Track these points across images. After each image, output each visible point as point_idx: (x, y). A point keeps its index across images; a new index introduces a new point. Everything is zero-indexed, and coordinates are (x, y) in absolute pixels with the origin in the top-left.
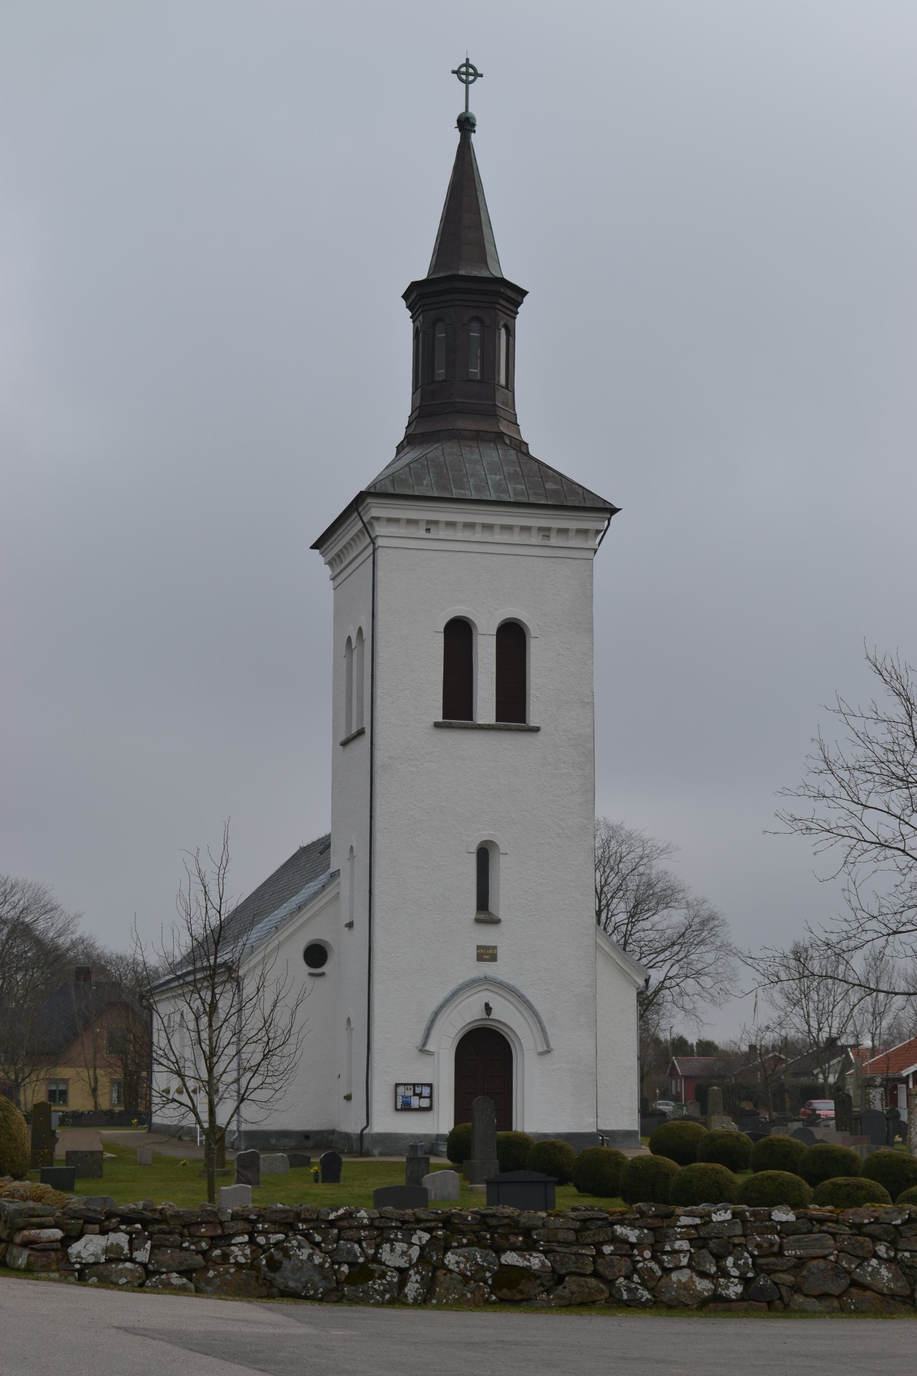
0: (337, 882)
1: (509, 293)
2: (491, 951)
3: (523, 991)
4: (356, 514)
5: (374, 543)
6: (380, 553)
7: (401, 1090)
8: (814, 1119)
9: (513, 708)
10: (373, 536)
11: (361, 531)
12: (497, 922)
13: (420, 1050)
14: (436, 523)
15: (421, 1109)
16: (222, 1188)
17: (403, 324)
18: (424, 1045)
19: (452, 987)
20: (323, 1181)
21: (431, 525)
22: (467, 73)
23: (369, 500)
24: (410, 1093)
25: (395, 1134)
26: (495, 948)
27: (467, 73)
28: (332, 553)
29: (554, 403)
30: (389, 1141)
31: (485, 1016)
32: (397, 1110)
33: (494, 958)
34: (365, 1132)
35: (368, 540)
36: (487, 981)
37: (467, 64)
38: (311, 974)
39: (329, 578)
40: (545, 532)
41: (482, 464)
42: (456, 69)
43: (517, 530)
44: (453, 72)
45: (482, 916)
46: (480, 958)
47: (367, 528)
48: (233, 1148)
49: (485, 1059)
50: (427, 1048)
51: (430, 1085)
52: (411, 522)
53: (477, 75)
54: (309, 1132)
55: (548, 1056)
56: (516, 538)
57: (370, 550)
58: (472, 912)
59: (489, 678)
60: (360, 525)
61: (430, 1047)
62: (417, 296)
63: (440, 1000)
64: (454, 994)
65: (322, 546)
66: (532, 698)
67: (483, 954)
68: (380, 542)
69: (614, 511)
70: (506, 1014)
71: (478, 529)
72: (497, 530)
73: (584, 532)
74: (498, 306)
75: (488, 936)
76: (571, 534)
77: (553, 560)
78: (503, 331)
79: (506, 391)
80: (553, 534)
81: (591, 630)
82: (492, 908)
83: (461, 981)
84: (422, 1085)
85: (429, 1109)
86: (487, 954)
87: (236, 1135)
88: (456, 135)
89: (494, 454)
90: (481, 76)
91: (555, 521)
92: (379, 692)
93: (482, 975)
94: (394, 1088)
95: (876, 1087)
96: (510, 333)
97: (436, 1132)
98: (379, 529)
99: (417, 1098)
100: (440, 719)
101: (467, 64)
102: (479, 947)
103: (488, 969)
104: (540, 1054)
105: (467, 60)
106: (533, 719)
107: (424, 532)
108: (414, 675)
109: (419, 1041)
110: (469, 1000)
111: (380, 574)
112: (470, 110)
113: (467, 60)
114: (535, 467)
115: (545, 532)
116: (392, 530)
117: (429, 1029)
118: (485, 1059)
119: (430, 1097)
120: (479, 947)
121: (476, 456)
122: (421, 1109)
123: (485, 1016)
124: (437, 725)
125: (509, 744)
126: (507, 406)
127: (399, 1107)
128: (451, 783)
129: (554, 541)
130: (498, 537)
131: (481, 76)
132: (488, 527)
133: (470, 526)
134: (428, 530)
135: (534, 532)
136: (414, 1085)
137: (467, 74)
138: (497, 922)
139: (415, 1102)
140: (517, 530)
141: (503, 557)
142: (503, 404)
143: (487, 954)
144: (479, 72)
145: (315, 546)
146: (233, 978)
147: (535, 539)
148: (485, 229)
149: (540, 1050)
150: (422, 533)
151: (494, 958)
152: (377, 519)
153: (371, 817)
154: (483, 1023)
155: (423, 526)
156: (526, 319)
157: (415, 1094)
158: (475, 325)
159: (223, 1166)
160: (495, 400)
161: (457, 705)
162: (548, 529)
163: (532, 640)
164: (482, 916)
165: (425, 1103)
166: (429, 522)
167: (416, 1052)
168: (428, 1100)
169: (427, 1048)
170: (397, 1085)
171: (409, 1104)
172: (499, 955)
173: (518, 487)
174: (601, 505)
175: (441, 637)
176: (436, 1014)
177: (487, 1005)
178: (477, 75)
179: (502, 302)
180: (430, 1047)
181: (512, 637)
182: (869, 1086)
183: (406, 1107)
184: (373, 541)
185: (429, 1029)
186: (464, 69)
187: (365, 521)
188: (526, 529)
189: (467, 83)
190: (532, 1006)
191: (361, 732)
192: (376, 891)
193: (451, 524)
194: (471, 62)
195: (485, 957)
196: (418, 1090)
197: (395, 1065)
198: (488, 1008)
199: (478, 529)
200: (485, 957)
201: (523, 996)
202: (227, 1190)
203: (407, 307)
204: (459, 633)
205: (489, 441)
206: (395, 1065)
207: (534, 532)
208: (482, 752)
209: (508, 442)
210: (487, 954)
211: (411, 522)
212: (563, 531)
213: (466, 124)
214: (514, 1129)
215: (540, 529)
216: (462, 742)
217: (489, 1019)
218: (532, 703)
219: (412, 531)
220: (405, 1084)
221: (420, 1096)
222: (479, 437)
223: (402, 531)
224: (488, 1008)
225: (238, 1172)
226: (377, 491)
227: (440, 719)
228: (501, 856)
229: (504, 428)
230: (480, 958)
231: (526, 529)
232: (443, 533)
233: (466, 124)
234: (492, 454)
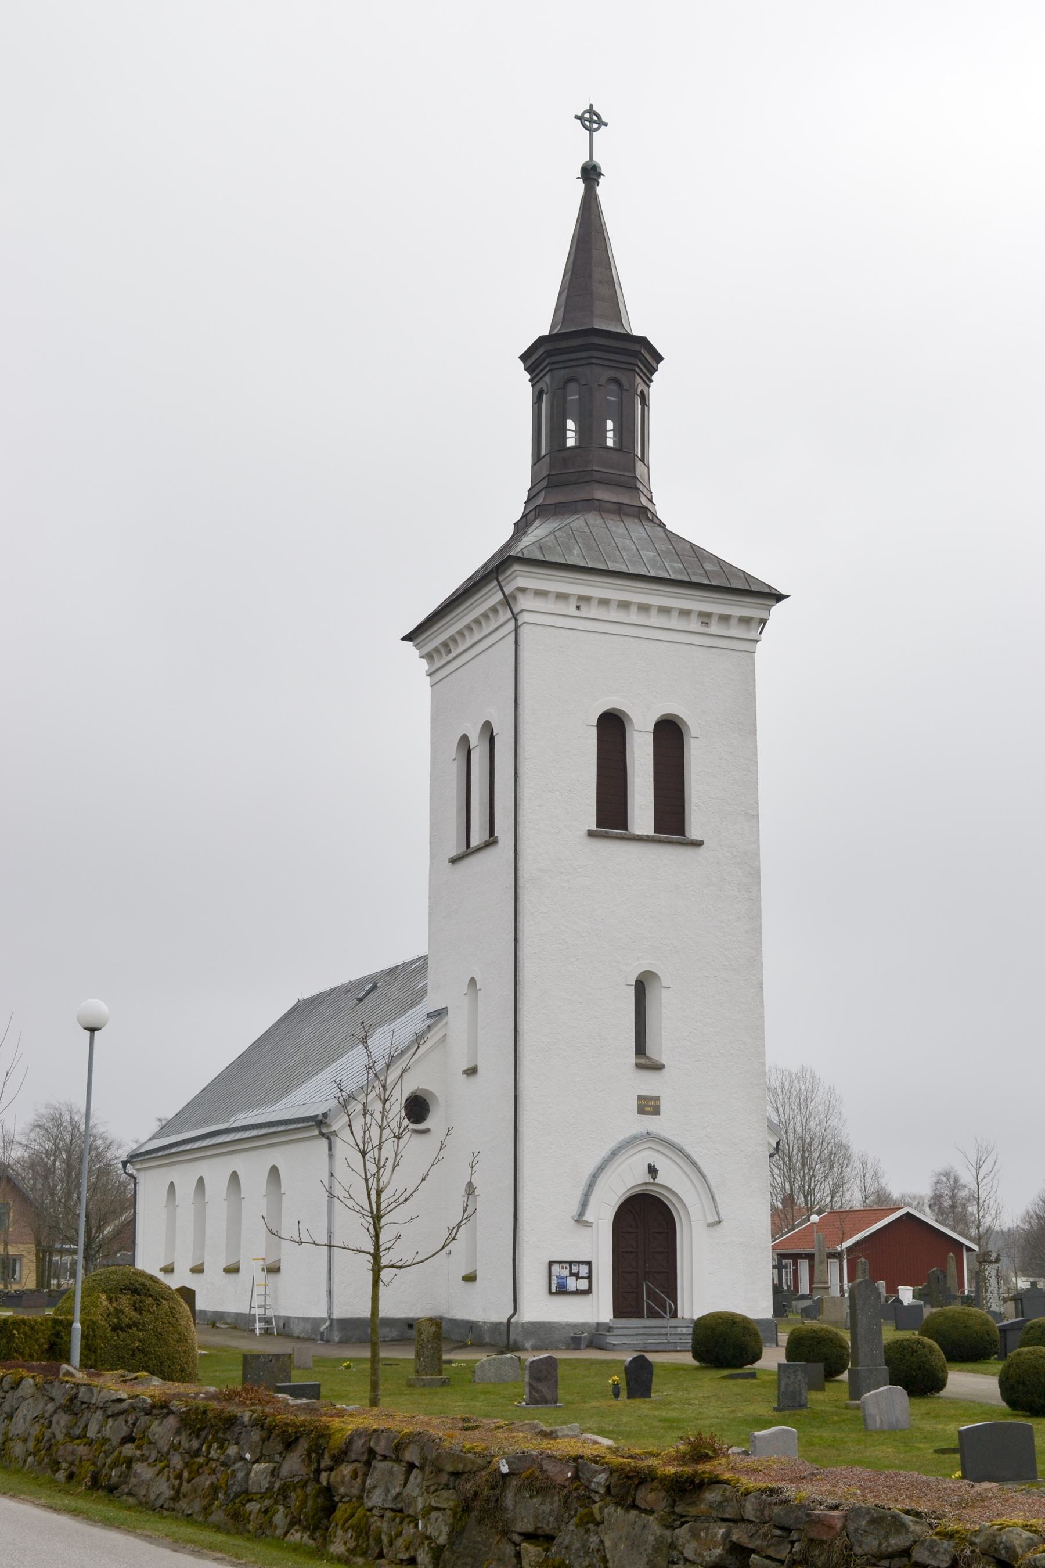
0: (444, 1022)
2: (653, 1103)
3: (688, 1149)
4: (495, 583)
5: (516, 620)
6: (524, 631)
9: (671, 819)
10: (516, 610)
11: (500, 603)
13: (577, 1221)
14: (587, 599)
16: (757, 1433)
17: (520, 387)
18: (582, 1213)
19: (612, 1145)
20: (630, 1396)
22: (591, 120)
23: (516, 567)
24: (566, 1273)
25: (549, 1323)
26: (657, 1098)
27: (591, 120)
28: (429, 648)
30: (543, 1333)
32: (551, 1293)
33: (656, 1111)
34: (512, 1320)
35: (509, 615)
36: (650, 1137)
37: (591, 111)
39: (424, 673)
40: (705, 617)
41: (624, 541)
44: (577, 117)
45: (643, 1061)
46: (641, 1111)
47: (508, 601)
48: (322, 1340)
49: (646, 1231)
50: (585, 1218)
51: (589, 1263)
52: (562, 597)
53: (601, 123)
54: (413, 1319)
55: (718, 1228)
57: (511, 625)
58: (630, 1056)
59: (647, 782)
60: (499, 596)
61: (588, 1217)
62: (540, 358)
63: (597, 1161)
64: (614, 1154)
65: (417, 637)
66: (693, 807)
67: (645, 1106)
68: (524, 617)
69: (779, 597)
70: (673, 1179)
72: (654, 612)
73: (746, 621)
75: (649, 1084)
77: (712, 650)
78: (638, 400)
80: (714, 621)
81: (754, 732)
82: (648, 1053)
84: (579, 1262)
85: (588, 1292)
86: (649, 1106)
87: (327, 1324)
88: (579, 188)
89: (641, 530)
90: (606, 124)
91: (717, 606)
92: (525, 793)
95: (991, 1262)
96: (644, 402)
97: (595, 1320)
98: (524, 602)
99: (574, 1278)
100: (594, 827)
101: (591, 111)
102: (640, 1098)
104: (710, 1225)
105: (591, 106)
106: (694, 829)
107: (575, 608)
108: (560, 778)
109: (575, 1209)
110: (627, 1163)
111: (525, 654)
112: (595, 159)
113: (591, 106)
114: (688, 547)
115: (705, 617)
116: (538, 604)
118: (646, 1231)
119: (589, 1278)
120: (640, 1098)
121: (622, 530)
124: (591, 834)
127: (554, 1290)
128: (606, 902)
129: (715, 628)
130: (655, 620)
131: (606, 124)
132: (644, 608)
133: (624, 605)
134: (578, 608)
136: (570, 1263)
137: (591, 121)
138: (658, 1067)
139: (572, 1284)
140: (675, 614)
143: (649, 1106)
145: (408, 638)
146: (323, 1135)
147: (694, 625)
149: (710, 1221)
150: (572, 610)
151: (656, 1111)
152: (523, 590)
153: (516, 940)
154: (644, 1188)
155: (573, 602)
156: (661, 387)
157: (571, 1274)
158: (613, 387)
159: (440, 1372)
161: (612, 814)
162: (709, 615)
163: (692, 741)
164: (643, 1061)
165: (583, 1285)
167: (573, 1222)
168: (586, 1281)
169: (585, 1218)
170: (589, 1263)
171: (564, 1286)
173: (675, 565)
174: (767, 590)
175: (594, 732)
176: (594, 1177)
178: (601, 123)
181: (670, 734)
182: (985, 1261)
183: (562, 1291)
184: (515, 617)
186: (587, 115)
187: (507, 593)
188: (685, 613)
189: (591, 131)
191: (492, 841)
192: (523, 1028)
193: (604, 602)
194: (595, 109)
195: (647, 1109)
196: (575, 1269)
198: (652, 1170)
199: (634, 609)
200: (647, 1109)
202: (762, 1437)
203: (526, 369)
204: (612, 727)
207: (694, 617)
208: (639, 865)
210: (649, 1106)
211: (562, 597)
212: (725, 619)
213: (590, 174)
218: (693, 812)
220: (560, 1262)
221: (577, 1276)
222: (621, 510)
223: (551, 606)
224: (652, 1170)
225: (531, 1385)
226: (526, 556)
227: (594, 827)
228: (663, 990)
230: (641, 1111)
231: (685, 613)
232: (595, 612)
233: (590, 174)
234: (638, 530)
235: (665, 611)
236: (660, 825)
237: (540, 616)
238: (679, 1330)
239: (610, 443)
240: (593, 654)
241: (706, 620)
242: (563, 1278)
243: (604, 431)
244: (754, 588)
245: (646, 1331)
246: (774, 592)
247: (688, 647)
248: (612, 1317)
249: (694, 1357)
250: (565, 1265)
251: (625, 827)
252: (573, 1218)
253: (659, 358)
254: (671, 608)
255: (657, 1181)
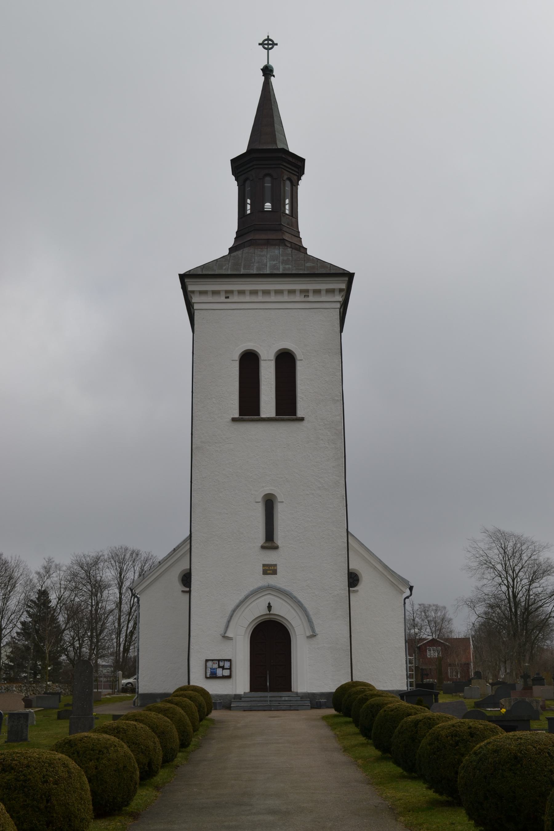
1: (291, 159)
2: (273, 568)
3: (295, 594)
7: (210, 664)
8: (493, 680)
9: (287, 407)
12: (276, 548)
14: (232, 292)
15: (224, 677)
18: (225, 633)
21: (228, 294)
24: (216, 666)
26: (275, 565)
29: (322, 223)
31: (268, 612)
32: (206, 678)
33: (275, 572)
38: (183, 591)
40: (305, 292)
41: (270, 258)
42: (261, 42)
43: (286, 293)
45: (267, 545)
46: (265, 573)
51: (230, 660)
52: (215, 293)
53: (274, 44)
55: (314, 639)
56: (286, 298)
59: (268, 389)
64: (247, 598)
67: (267, 570)
70: (283, 610)
71: (260, 294)
74: (281, 166)
75: (270, 558)
76: (323, 293)
79: (291, 218)
80: (311, 294)
83: (252, 589)
85: (229, 677)
86: (270, 570)
88: (261, 79)
93: (266, 584)
94: (205, 663)
97: (234, 693)
99: (221, 669)
100: (237, 415)
101: (268, 39)
103: (270, 580)
106: (300, 414)
107: (224, 298)
109: (222, 632)
112: (270, 63)
115: (305, 292)
116: (203, 298)
117: (229, 622)
119: (230, 669)
122: (224, 677)
123: (268, 612)
124: (234, 420)
125: (284, 430)
126: (292, 226)
127: (208, 675)
130: (273, 298)
135: (298, 293)
136: (219, 660)
139: (219, 672)
141: (277, 310)
142: (288, 224)
143: (270, 570)
144: (275, 42)
147: (298, 298)
148: (277, 126)
149: (308, 634)
150: (223, 299)
151: (275, 572)
154: (268, 617)
157: (219, 667)
158: (268, 179)
160: (281, 222)
161: (249, 407)
162: (307, 291)
163: (196, 311)
165: (226, 673)
166: (227, 292)
167: (221, 637)
168: (228, 671)
170: (207, 661)
172: (278, 570)
174: (341, 272)
175: (236, 365)
176: (234, 611)
177: (269, 604)
178: (274, 44)
179: (285, 164)
180: (229, 634)
181: (286, 362)
183: (213, 676)
185: (229, 622)
188: (292, 292)
189: (268, 49)
190: (302, 604)
195: (268, 572)
196: (221, 664)
197: (206, 648)
198: (269, 607)
200: (268, 572)
201: (295, 597)
204: (249, 362)
205: (275, 245)
206: (206, 648)
207: (298, 293)
208: (267, 437)
209: (289, 245)
210: (270, 570)
211: (215, 293)
213: (268, 71)
214: (294, 689)
215: (302, 291)
216: (252, 429)
217: (270, 614)
219: (216, 299)
221: (223, 668)
222: (268, 243)
223: (209, 298)
224: (269, 607)
227: (237, 415)
229: (287, 237)
230: (265, 573)
233: (268, 71)
235: (279, 292)
236: (279, 411)
237: (211, 305)
238: (283, 699)
239: (287, 212)
240: (267, 323)
241: (307, 294)
242: (214, 669)
243: (285, 205)
244: (332, 272)
245: (262, 699)
246: (346, 272)
247: (295, 310)
248: (247, 690)
249: (336, 710)
250: (215, 662)
251: (258, 414)
252: (221, 635)
253: (303, 160)
254: (257, 290)
255: (271, 612)
